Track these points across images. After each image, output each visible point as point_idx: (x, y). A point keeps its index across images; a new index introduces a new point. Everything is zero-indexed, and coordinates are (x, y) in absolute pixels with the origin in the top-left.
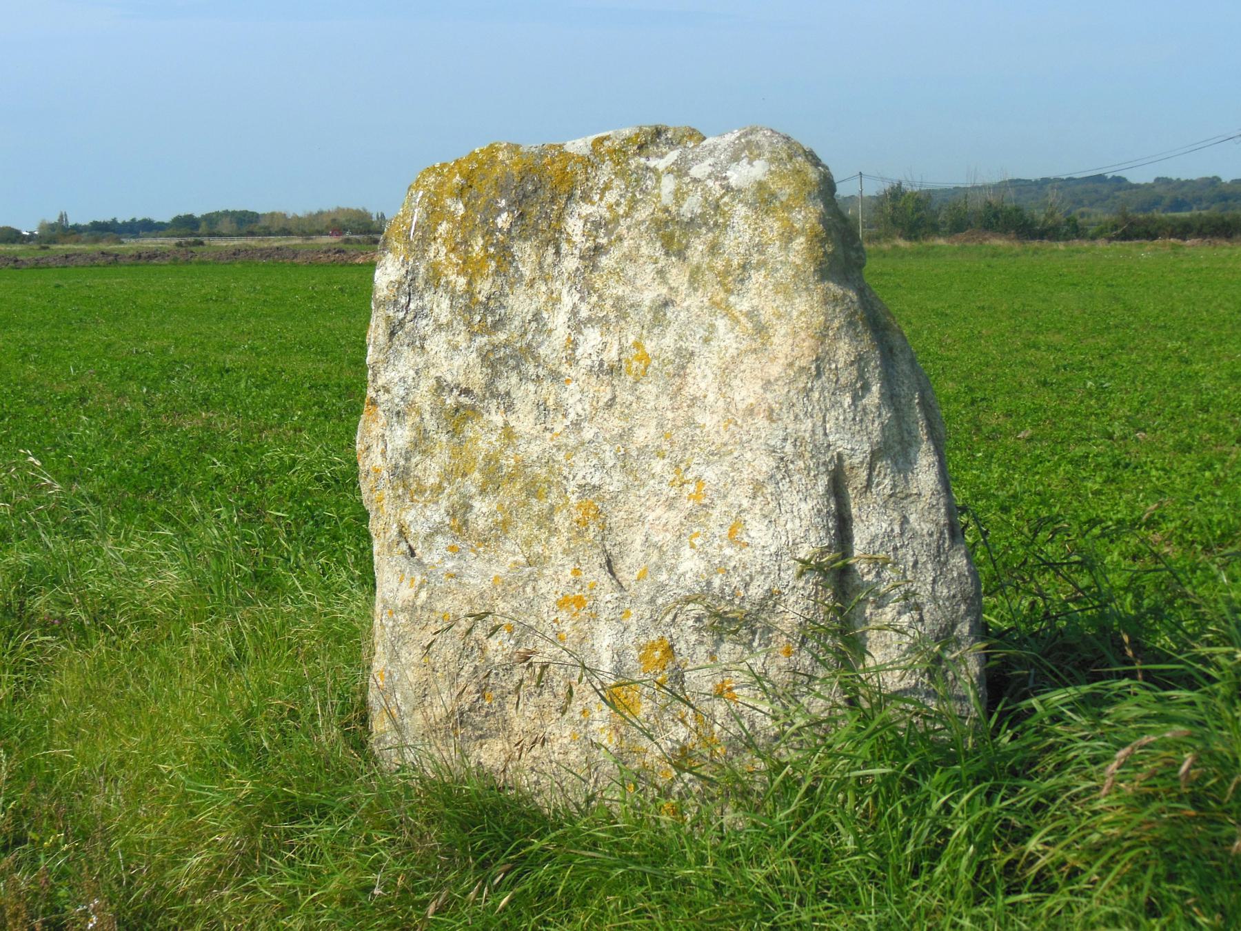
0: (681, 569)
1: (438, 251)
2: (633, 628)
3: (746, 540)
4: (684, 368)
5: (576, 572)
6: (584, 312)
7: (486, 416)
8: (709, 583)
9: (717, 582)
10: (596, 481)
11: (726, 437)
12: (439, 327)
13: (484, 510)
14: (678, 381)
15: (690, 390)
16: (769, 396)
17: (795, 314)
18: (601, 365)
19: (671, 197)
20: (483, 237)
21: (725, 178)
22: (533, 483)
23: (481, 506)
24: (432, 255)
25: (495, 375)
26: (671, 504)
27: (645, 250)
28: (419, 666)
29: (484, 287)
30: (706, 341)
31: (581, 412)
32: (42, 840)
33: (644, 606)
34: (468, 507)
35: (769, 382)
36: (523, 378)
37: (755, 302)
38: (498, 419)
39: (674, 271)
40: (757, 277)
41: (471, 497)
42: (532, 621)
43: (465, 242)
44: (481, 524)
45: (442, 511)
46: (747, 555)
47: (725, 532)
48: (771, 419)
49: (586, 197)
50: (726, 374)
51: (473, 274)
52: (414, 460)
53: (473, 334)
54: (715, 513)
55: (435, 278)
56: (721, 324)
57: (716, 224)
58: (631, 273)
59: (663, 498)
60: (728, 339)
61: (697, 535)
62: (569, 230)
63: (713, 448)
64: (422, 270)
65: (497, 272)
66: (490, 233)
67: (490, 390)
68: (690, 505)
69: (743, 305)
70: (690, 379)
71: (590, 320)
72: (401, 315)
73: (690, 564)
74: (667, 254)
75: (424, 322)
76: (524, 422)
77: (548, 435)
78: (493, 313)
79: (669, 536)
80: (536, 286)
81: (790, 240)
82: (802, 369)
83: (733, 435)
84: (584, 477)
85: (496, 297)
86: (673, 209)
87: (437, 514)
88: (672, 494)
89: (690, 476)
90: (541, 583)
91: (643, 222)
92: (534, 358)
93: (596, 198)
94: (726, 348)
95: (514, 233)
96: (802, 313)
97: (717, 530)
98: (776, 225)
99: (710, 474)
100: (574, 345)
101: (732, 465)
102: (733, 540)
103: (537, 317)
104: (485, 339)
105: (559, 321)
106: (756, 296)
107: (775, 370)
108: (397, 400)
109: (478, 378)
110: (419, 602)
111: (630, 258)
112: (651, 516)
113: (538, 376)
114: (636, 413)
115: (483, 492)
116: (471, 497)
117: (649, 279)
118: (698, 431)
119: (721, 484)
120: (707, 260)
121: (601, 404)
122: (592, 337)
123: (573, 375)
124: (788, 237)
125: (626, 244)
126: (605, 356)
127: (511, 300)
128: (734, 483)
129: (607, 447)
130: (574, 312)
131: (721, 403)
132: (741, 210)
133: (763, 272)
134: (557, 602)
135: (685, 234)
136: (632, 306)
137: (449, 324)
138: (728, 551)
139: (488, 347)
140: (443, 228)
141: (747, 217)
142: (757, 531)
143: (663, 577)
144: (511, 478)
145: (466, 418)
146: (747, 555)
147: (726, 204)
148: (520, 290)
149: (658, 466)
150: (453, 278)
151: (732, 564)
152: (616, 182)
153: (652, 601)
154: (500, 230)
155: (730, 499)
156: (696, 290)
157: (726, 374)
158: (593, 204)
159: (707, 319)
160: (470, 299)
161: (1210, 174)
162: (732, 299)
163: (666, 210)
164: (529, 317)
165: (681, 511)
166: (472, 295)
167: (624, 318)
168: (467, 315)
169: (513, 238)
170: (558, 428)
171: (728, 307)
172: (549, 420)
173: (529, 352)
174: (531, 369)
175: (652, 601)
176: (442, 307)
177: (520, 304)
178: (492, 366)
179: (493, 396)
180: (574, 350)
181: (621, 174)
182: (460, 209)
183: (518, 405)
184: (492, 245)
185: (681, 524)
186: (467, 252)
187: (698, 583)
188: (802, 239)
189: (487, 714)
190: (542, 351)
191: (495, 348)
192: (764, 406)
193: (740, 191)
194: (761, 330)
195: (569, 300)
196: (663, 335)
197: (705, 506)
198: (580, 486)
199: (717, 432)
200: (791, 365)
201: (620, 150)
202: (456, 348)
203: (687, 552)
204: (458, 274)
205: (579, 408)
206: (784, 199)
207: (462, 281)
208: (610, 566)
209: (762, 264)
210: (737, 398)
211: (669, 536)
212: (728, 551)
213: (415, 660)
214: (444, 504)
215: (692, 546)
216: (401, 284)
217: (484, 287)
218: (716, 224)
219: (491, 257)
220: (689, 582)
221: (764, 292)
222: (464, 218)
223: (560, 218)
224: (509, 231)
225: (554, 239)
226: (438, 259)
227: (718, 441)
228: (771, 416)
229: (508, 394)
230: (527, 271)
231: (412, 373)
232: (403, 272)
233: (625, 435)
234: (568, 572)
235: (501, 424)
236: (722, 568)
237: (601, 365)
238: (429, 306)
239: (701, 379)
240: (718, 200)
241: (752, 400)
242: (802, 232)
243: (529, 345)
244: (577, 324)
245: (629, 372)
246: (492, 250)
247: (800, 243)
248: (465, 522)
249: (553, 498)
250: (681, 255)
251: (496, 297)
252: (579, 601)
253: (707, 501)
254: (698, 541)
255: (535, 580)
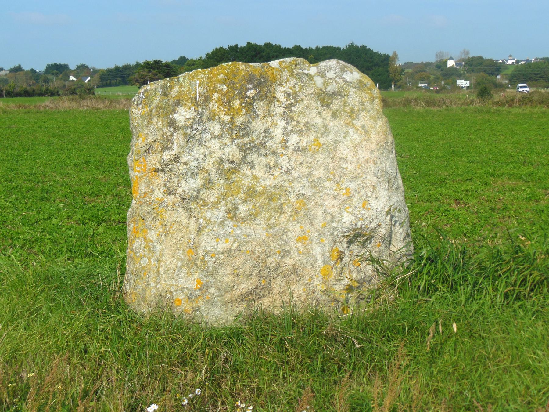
0: (344, 221)
1: (213, 106)
2: (327, 245)
3: (370, 207)
4: (336, 147)
5: (301, 227)
6: (290, 128)
7: (242, 171)
8: (356, 225)
9: (359, 224)
10: (303, 192)
11: (359, 171)
12: (214, 137)
13: (245, 209)
14: (334, 152)
15: (339, 155)
16: (373, 155)
17: (378, 126)
18: (299, 148)
19: (322, 85)
20: (239, 100)
21: (344, 78)
22: (271, 196)
23: (243, 208)
24: (211, 107)
25: (246, 155)
26: (335, 198)
27: (313, 104)
28: (230, 274)
29: (239, 120)
30: (344, 137)
31: (289, 167)
32: (471, 275)
33: (329, 236)
34: (236, 208)
35: (372, 151)
36: (260, 155)
37: (363, 123)
38: (248, 172)
39: (324, 112)
40: (363, 114)
41: (238, 204)
42: (288, 248)
43: (229, 101)
44: (243, 215)
45: (223, 211)
46: (371, 212)
47: (361, 205)
48: (374, 164)
49: (281, 84)
50: (355, 149)
51: (234, 115)
52: (202, 192)
53: (233, 140)
54: (355, 199)
55: (212, 117)
56: (351, 131)
57: (345, 95)
58: (308, 113)
59: (331, 196)
60: (354, 136)
61: (348, 208)
62: (278, 97)
63: (353, 175)
64: (206, 113)
65: (246, 114)
66: (244, 98)
67: (244, 161)
68: (344, 197)
69: (358, 124)
70: (338, 151)
71: (292, 131)
72: (194, 132)
73: (348, 219)
74: (322, 106)
75: (206, 135)
76: (259, 172)
77: (272, 177)
78: (243, 130)
79: (335, 209)
80: (266, 119)
81: (373, 100)
82: (381, 145)
83: (362, 170)
84: (299, 191)
85: (247, 124)
86: (323, 89)
87: (221, 213)
88: (336, 194)
89: (343, 187)
90: (289, 233)
91: (312, 94)
92: (263, 147)
93: (285, 84)
94: (355, 140)
95: (256, 98)
96: (380, 126)
97: (357, 205)
98: (367, 95)
99: (352, 185)
100: (286, 141)
101: (362, 181)
102: (365, 208)
103: (266, 131)
104: (240, 141)
105: (278, 133)
106: (363, 120)
107: (374, 146)
108: (192, 168)
109: (238, 156)
110: (233, 248)
111: (308, 107)
112: (326, 203)
113: (266, 154)
114: (313, 165)
115: (244, 201)
116: (238, 204)
117: (314, 115)
118: (345, 170)
119: (357, 188)
120: (342, 108)
121: (298, 163)
122: (294, 139)
123: (284, 152)
124: (372, 99)
125: (305, 102)
126: (300, 145)
127: (253, 124)
128: (363, 187)
129: (305, 179)
130: (285, 128)
131: (355, 159)
132: (352, 90)
133: (364, 112)
134: (296, 239)
135: (330, 99)
136: (312, 125)
137: (220, 136)
138: (363, 212)
139: (241, 144)
140: (216, 96)
141: (356, 92)
142: (373, 203)
143: (335, 225)
144: (260, 195)
145: (233, 173)
146: (371, 212)
147: (346, 88)
148: (257, 121)
149: (328, 184)
150: (222, 116)
151: (366, 216)
152: (291, 79)
153: (332, 234)
154: (249, 97)
155: (362, 193)
156: (335, 119)
157: (355, 149)
158: (284, 87)
159: (345, 129)
160: (232, 125)
161: (298, 45)
162: (355, 122)
163: (321, 90)
164: (262, 131)
165: (340, 200)
166: (233, 123)
167: (309, 130)
168: (230, 132)
169: (255, 100)
170: (276, 174)
171: (353, 124)
172: (271, 171)
173: (262, 145)
174: (263, 151)
175: (332, 234)
176: (216, 128)
177: (258, 126)
178: (244, 151)
179: (245, 163)
180: (286, 143)
181: (292, 75)
182: (225, 88)
183: (256, 166)
184: (244, 103)
185: (340, 204)
186: (230, 106)
187: (351, 225)
188: (377, 100)
189: (263, 288)
190: (268, 144)
191: (245, 144)
192: (372, 160)
193: (351, 83)
194: (367, 132)
195: (282, 124)
196: (328, 136)
197: (351, 197)
198: (297, 195)
199: (355, 170)
200: (378, 144)
201: (289, 67)
202: (226, 145)
203: (345, 214)
204: (225, 114)
205: (288, 165)
206: (368, 86)
207: (227, 118)
208: (311, 223)
209: (364, 109)
210: (361, 157)
211: (335, 209)
212: (363, 212)
213: (229, 272)
214: (223, 208)
215: (348, 212)
216: (194, 119)
217: (239, 120)
218: (345, 95)
219: (244, 108)
220: (347, 225)
221: (366, 119)
222: (227, 92)
223: (274, 93)
224: (253, 97)
225: (272, 99)
226: (213, 109)
227: (356, 173)
228: (375, 163)
229: (252, 162)
230: (261, 113)
231: (202, 156)
232: (195, 114)
233: (310, 174)
234: (298, 227)
235: (250, 174)
236: (362, 218)
237: (299, 148)
238: (208, 128)
239: (344, 151)
240: (343, 86)
241: (367, 158)
242: (377, 98)
243: (261, 142)
244: (287, 133)
245: (310, 150)
246: (244, 105)
247: (377, 101)
248: (235, 215)
249: (283, 199)
250: (328, 106)
251: (247, 124)
252: (305, 238)
253: (352, 195)
254: (350, 210)
255: (286, 232)
